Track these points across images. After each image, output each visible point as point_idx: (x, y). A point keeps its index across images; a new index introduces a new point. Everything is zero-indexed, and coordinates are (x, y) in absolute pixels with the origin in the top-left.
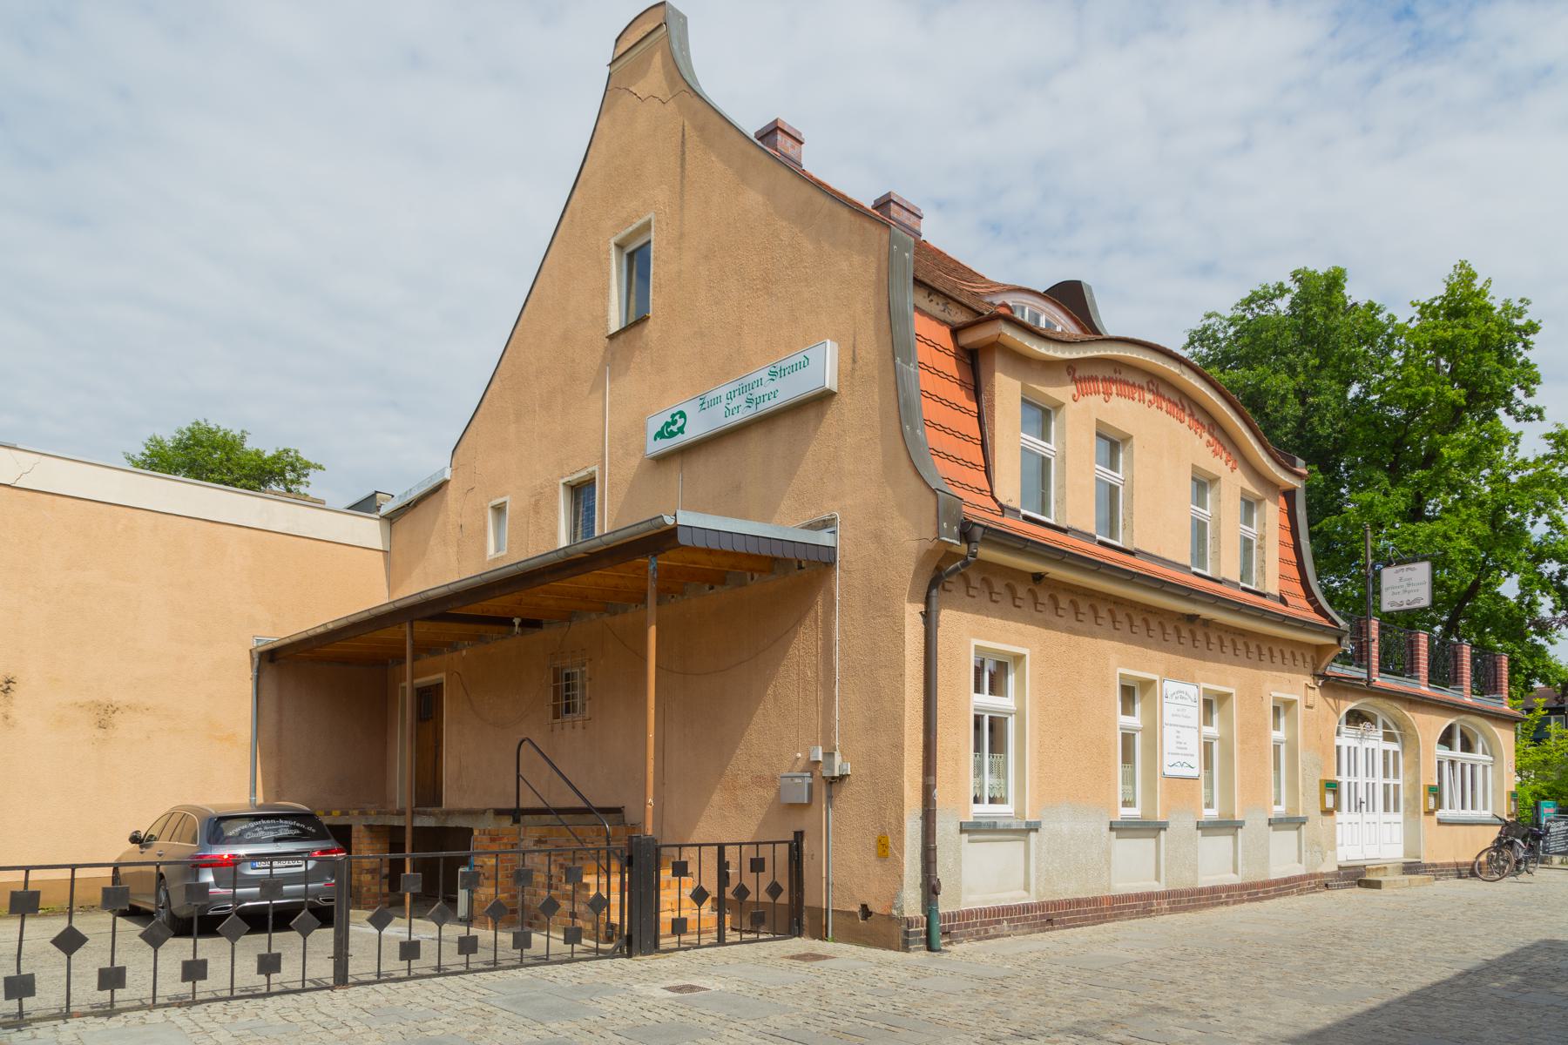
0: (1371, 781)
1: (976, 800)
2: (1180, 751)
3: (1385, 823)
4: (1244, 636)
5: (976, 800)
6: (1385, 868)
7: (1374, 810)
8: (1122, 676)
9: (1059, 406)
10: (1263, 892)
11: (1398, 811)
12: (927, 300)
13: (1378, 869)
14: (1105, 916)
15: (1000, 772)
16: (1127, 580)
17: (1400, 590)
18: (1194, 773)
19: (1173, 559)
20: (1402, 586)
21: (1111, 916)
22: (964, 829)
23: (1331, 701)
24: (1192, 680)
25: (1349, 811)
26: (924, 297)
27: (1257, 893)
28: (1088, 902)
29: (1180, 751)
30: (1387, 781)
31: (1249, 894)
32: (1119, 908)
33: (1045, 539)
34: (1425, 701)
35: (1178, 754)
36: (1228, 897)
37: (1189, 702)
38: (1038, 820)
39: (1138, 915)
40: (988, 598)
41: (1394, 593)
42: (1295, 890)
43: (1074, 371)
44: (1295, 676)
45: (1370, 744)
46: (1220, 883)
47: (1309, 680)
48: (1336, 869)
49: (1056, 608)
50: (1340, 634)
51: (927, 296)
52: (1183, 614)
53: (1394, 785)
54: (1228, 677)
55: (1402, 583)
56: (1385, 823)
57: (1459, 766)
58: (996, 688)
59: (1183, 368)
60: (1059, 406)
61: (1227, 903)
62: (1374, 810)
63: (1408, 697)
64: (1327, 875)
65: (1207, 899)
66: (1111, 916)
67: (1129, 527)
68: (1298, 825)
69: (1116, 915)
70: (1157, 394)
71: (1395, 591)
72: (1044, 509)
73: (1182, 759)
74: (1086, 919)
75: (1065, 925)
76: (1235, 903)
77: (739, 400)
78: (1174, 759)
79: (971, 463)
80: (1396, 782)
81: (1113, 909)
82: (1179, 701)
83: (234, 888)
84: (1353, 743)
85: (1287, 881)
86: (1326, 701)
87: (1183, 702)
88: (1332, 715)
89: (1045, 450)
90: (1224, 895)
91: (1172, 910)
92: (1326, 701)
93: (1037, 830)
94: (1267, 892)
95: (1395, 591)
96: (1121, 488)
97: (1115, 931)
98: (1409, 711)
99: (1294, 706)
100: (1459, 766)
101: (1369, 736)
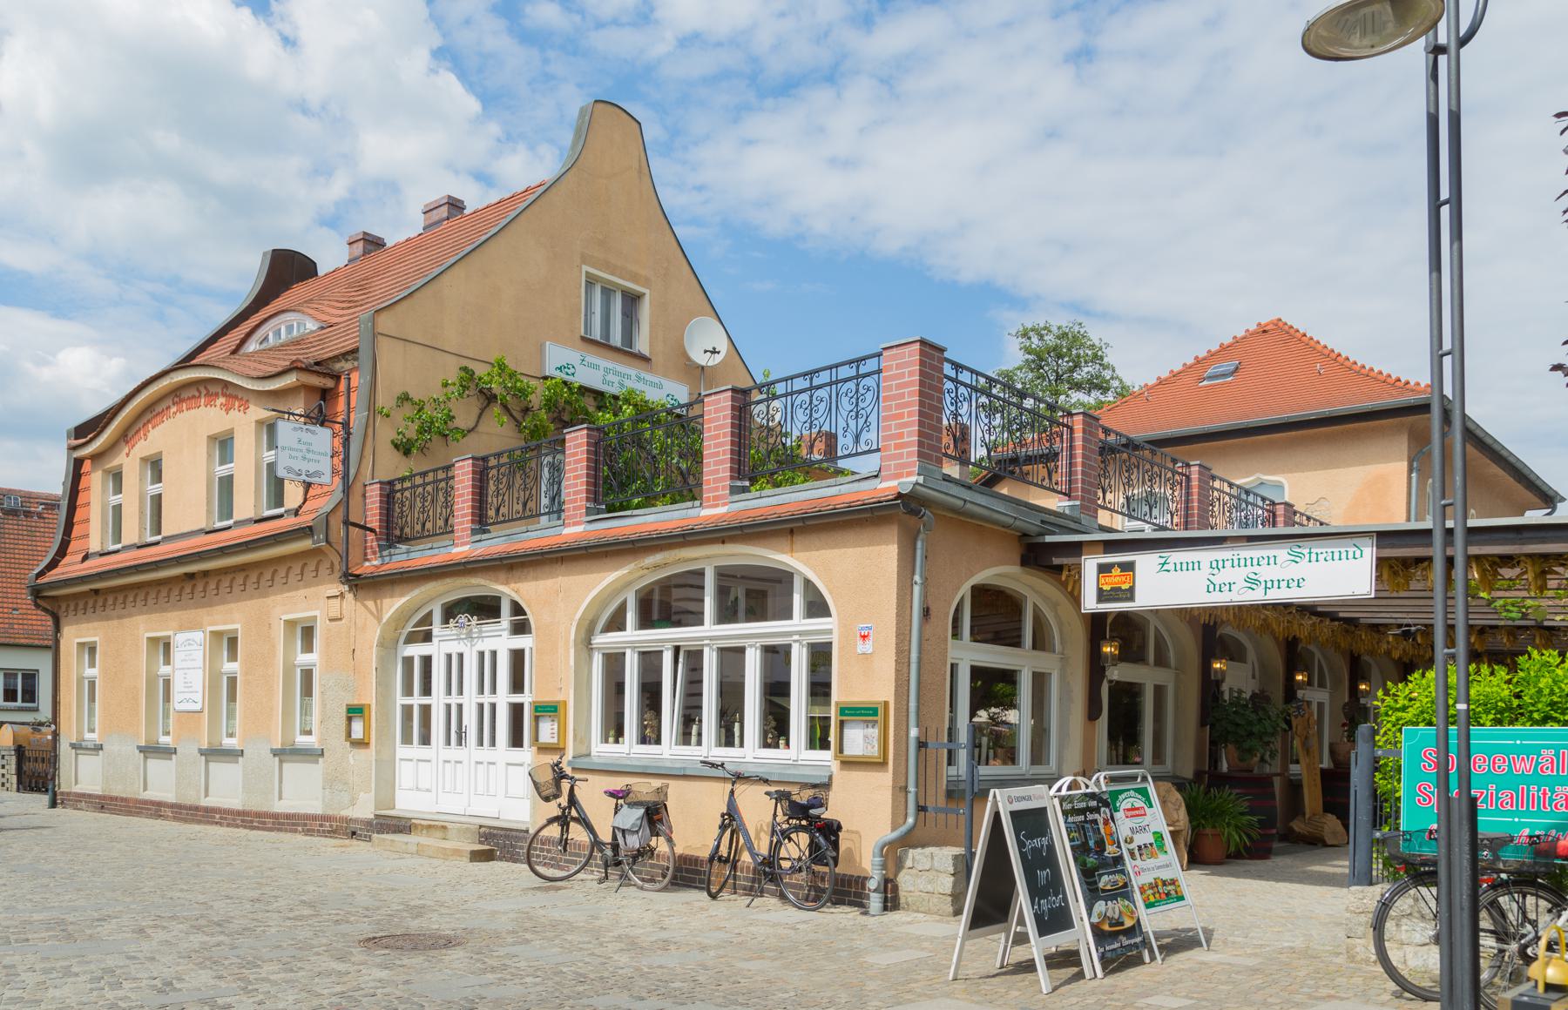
0: (487, 699)
2: (186, 690)
3: (429, 761)
4: (244, 570)
6: (444, 828)
9: (121, 466)
10: (258, 822)
13: (430, 827)
14: (131, 812)
17: (299, 454)
18: (198, 707)
20: (301, 451)
21: (135, 812)
23: (370, 604)
27: (252, 822)
28: (123, 799)
29: (186, 690)
30: (425, 700)
31: (243, 821)
32: (140, 808)
34: (405, 575)
36: (221, 818)
37: (195, 647)
39: (151, 816)
42: (300, 828)
43: (227, 389)
44: (313, 589)
45: (486, 645)
46: (302, 811)
47: (336, 588)
48: (952, 879)
53: (421, 706)
54: (233, 615)
55: (300, 447)
56: (429, 761)
58: (308, 647)
60: (121, 466)
61: (221, 824)
63: (505, 562)
64: (356, 821)
65: (203, 816)
66: (135, 812)
69: (138, 813)
71: (294, 454)
73: (188, 696)
74: (121, 811)
75: (112, 812)
76: (228, 825)
77: (616, 379)
80: (408, 701)
81: (136, 808)
82: (188, 648)
84: (454, 648)
85: (288, 816)
86: (366, 607)
88: (372, 621)
90: (218, 816)
91: (175, 819)
92: (366, 607)
93: (102, 749)
94: (264, 823)
95: (294, 454)
98: (507, 583)
100: (1017, 640)
101: (480, 632)
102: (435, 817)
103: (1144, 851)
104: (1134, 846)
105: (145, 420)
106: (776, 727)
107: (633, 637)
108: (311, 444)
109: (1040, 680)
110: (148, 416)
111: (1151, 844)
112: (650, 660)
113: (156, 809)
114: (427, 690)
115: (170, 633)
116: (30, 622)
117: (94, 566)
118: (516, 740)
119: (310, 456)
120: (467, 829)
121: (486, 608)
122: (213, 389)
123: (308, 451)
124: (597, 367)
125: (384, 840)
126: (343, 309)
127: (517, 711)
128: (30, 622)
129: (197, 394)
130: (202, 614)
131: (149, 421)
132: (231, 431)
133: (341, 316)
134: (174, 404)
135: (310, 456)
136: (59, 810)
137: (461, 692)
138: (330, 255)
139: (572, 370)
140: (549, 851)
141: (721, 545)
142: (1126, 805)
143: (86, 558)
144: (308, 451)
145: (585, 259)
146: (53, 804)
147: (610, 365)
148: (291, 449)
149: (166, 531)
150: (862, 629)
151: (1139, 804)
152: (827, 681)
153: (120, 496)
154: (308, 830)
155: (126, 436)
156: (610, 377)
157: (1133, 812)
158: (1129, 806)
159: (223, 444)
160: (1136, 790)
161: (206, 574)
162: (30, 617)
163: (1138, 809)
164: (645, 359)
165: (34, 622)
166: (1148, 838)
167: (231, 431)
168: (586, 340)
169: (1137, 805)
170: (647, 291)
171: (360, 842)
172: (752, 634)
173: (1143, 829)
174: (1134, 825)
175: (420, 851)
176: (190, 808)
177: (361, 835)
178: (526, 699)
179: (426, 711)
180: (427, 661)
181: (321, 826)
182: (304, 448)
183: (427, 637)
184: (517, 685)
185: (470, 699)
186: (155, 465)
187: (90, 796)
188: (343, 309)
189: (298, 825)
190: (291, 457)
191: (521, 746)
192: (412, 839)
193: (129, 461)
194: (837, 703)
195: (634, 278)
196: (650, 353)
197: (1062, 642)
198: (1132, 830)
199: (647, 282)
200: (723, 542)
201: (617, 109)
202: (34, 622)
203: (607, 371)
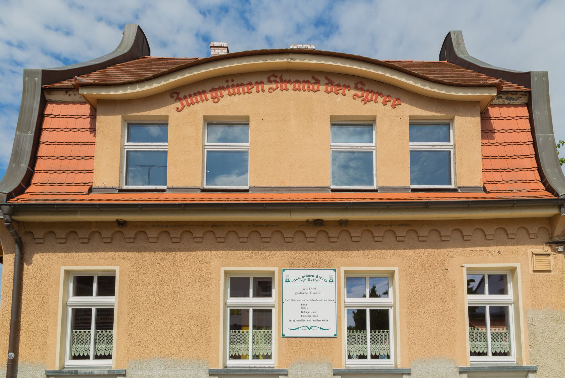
1: (350, 357)
5: (350, 357)
8: (346, 272)
12: (67, 96)
15: (506, 337)
16: (511, 206)
19: (269, 185)
24: (328, 266)
26: (64, 95)
33: (363, 199)
35: (305, 321)
38: (410, 368)
40: (528, 237)
49: (463, 236)
50: (560, 203)
51: (65, 93)
52: (546, 218)
59: (291, 56)
68: (525, 374)
70: (330, 83)
79: (493, 169)
89: (157, 147)
96: (374, 152)
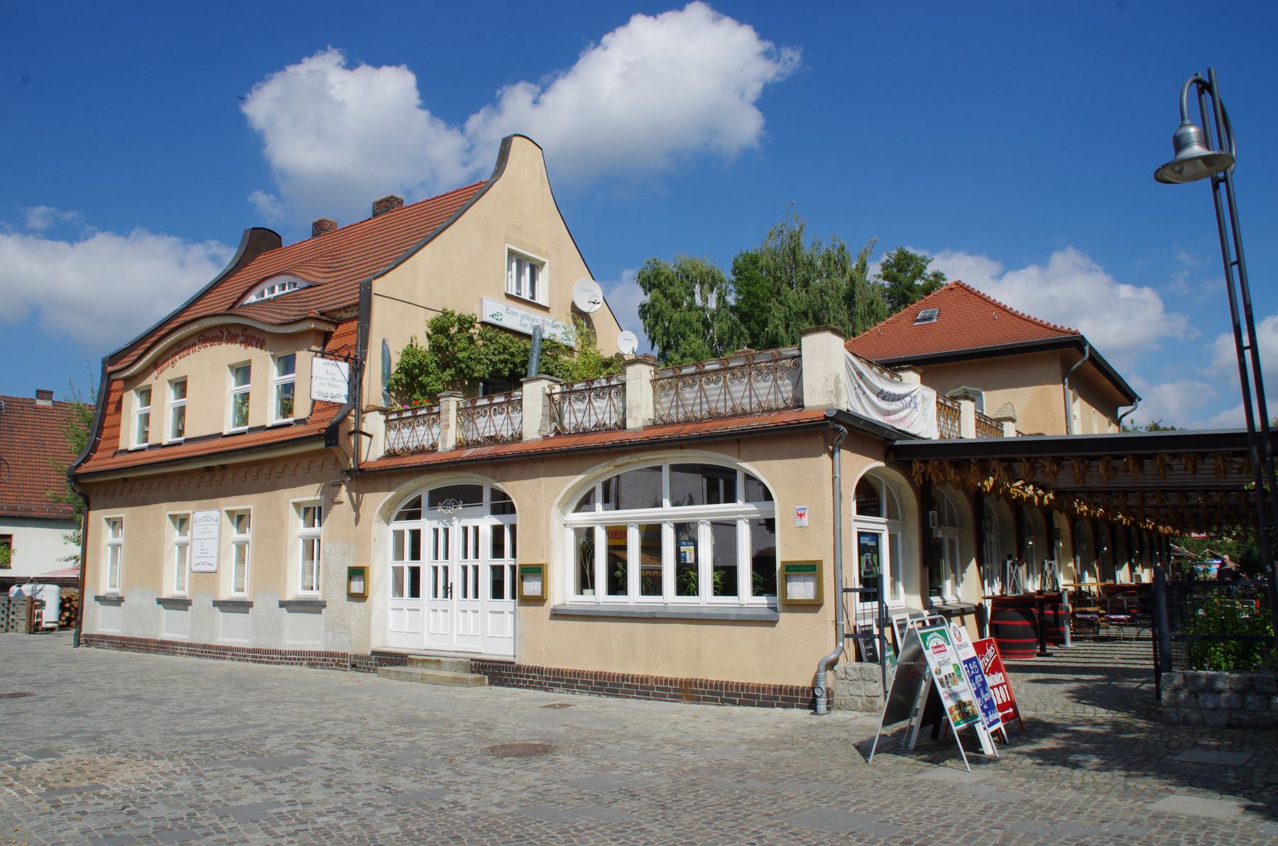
2: (203, 555)
7: (476, 596)
9: (151, 385)
11: (502, 597)
17: (326, 382)
22: (98, 598)
25: (465, 596)
29: (203, 555)
37: (212, 522)
41: (321, 384)
46: (114, 635)
57: (946, 521)
60: (151, 385)
62: (476, 596)
67: (536, 298)
69: (156, 651)
72: (533, 297)
78: (199, 561)
82: (205, 523)
83: (874, 636)
87: (208, 523)
95: (322, 381)
97: (512, 694)
99: (186, 523)
100: (946, 521)
102: (430, 653)
103: (949, 680)
104: (942, 676)
105: (173, 352)
106: (617, 585)
107: (600, 516)
108: (334, 374)
109: (952, 542)
110: (177, 349)
111: (953, 674)
112: (617, 535)
113: (221, 652)
114: (416, 555)
115: (190, 512)
116: (8, 497)
117: (121, 461)
118: (497, 592)
119: (334, 383)
120: (459, 662)
121: (469, 496)
122: (233, 331)
123: (333, 379)
124: (516, 314)
125: (389, 671)
126: (325, 273)
127: (497, 572)
128: (8, 497)
129: (220, 335)
130: (222, 501)
131: (177, 354)
132: (250, 361)
133: (326, 278)
134: (199, 341)
135: (334, 383)
136: (82, 649)
137: (477, 556)
138: (295, 233)
139: (500, 317)
140: (534, 677)
141: (680, 450)
142: (932, 644)
143: (115, 454)
144: (333, 379)
145: (507, 240)
146: (78, 644)
147: (525, 313)
148: (321, 378)
149: (189, 433)
150: (799, 509)
151: (941, 642)
152: (772, 546)
153: (148, 407)
154: (313, 664)
155: (156, 364)
156: (525, 321)
157: (939, 649)
158: (935, 645)
159: (243, 372)
160: (938, 631)
161: (223, 467)
162: (7, 493)
163: (940, 646)
164: (546, 309)
165: (11, 498)
166: (951, 670)
167: (250, 361)
168: (509, 296)
169: (940, 644)
170: (547, 261)
171: (360, 673)
172: (702, 511)
173: (946, 662)
174: (941, 660)
175: (423, 679)
176: (205, 646)
177: (360, 668)
178: (507, 561)
179: (415, 573)
180: (416, 535)
181: (324, 660)
182: (330, 377)
183: (415, 515)
184: (498, 550)
185: (456, 562)
186: (181, 387)
187: (112, 637)
188: (325, 273)
189: (303, 659)
190: (321, 384)
191: (502, 597)
192: (408, 669)
193: (160, 382)
194: (782, 563)
195: (538, 251)
196: (550, 303)
197: (903, 512)
198: (939, 663)
199: (547, 255)
200: (682, 448)
201: (526, 140)
202: (11, 498)
203: (523, 316)
